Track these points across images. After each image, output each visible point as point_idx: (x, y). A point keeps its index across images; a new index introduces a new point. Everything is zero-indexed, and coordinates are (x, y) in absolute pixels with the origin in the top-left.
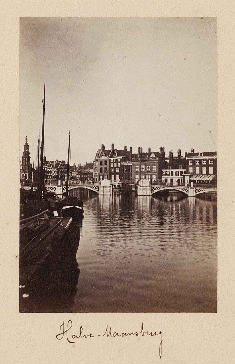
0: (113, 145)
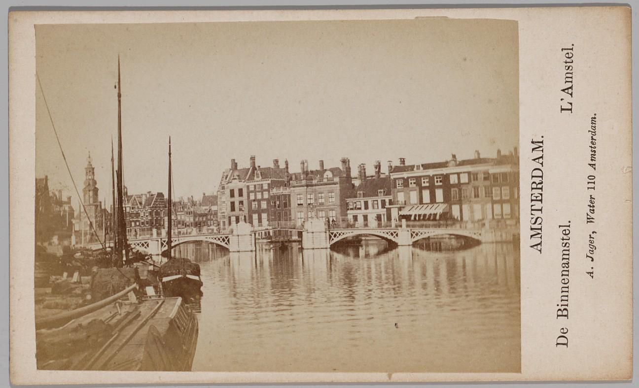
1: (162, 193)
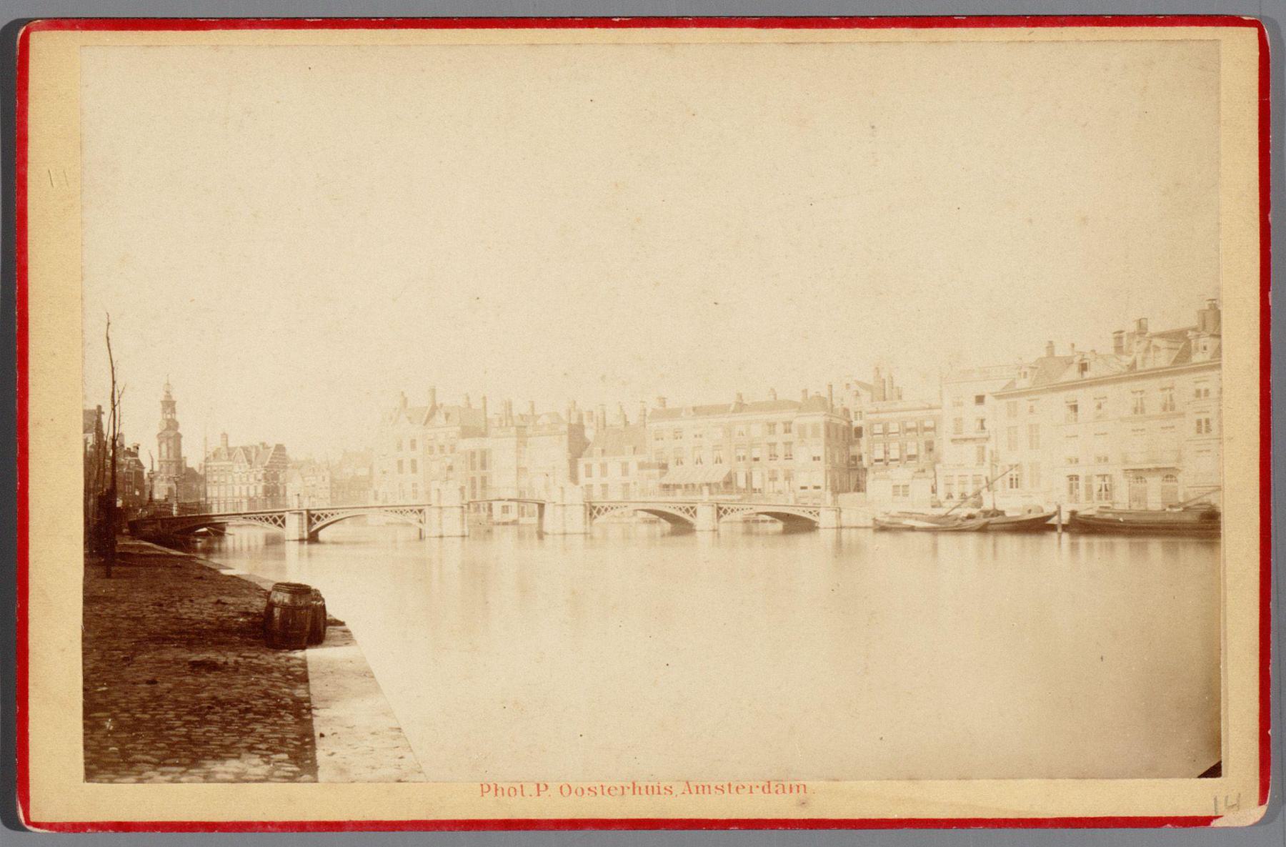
0: (225, 436)
1: (281, 445)
